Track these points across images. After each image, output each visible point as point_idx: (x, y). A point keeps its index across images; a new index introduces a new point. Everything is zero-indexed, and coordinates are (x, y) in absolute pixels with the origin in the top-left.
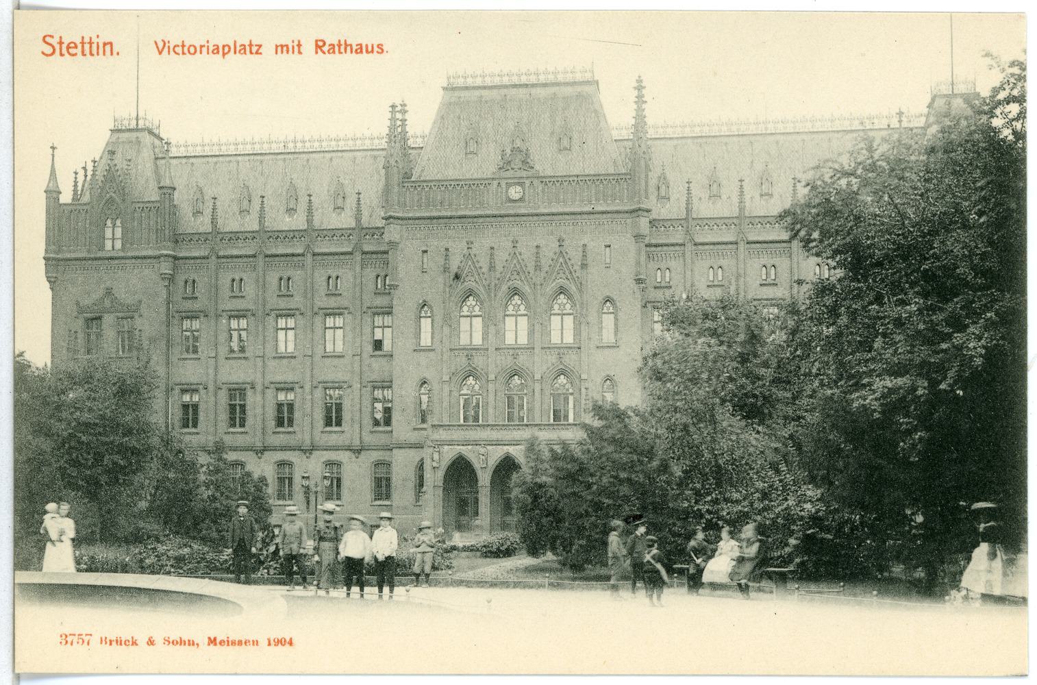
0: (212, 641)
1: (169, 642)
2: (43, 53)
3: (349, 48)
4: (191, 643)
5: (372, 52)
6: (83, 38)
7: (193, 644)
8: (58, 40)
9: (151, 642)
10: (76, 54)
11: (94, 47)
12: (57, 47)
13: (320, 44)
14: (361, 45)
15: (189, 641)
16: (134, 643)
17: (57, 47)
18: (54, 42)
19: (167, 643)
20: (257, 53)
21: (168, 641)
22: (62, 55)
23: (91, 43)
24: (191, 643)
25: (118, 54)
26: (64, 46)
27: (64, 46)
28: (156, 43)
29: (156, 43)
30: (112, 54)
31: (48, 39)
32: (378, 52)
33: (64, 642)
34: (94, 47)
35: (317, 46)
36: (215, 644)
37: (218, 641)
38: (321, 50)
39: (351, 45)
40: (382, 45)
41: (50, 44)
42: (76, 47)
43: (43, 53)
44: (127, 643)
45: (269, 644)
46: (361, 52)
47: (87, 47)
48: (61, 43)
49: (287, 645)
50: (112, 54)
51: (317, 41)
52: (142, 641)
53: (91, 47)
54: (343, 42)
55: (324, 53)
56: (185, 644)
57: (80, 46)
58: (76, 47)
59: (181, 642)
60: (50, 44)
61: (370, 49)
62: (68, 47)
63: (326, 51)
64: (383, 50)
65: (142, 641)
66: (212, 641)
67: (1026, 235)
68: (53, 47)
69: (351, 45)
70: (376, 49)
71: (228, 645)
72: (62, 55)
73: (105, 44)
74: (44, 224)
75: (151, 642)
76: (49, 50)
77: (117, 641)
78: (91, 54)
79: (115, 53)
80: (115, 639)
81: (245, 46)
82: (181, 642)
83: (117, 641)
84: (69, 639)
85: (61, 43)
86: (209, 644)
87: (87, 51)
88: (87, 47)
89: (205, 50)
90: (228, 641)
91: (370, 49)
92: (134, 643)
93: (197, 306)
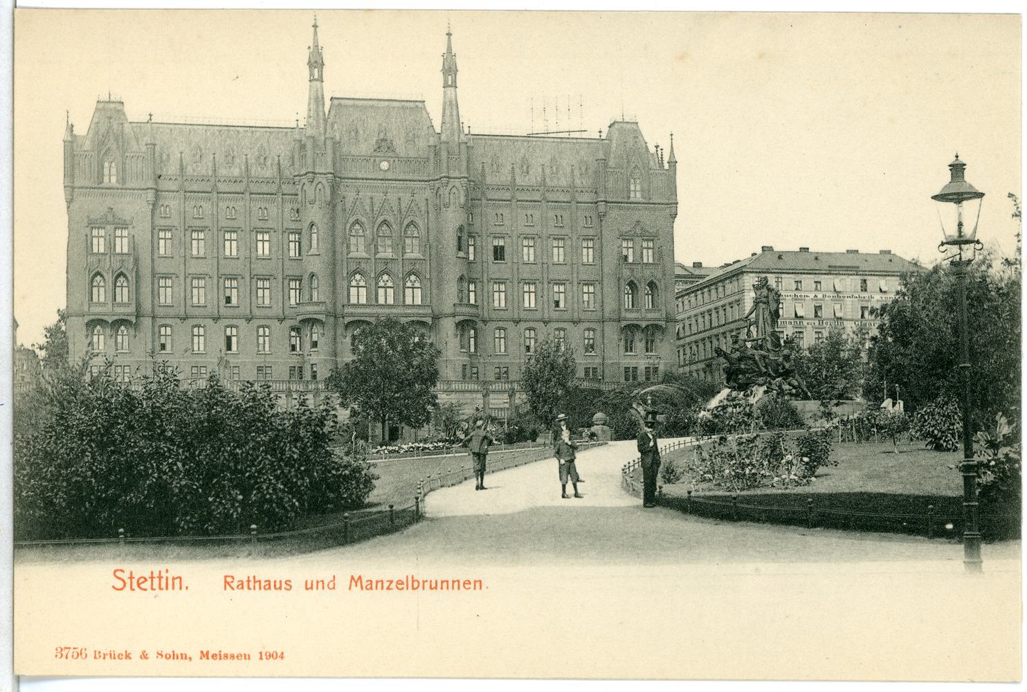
0: (204, 655)
1: (162, 656)
2: (113, 587)
4: (184, 657)
5: (280, 588)
6: (152, 573)
7: (186, 658)
8: (129, 575)
9: (144, 656)
10: (403, 588)
11: (163, 581)
12: (128, 582)
13: (229, 579)
14: (269, 581)
15: (182, 655)
16: (128, 656)
17: (128, 582)
18: (125, 576)
19: (160, 657)
21: (247, 657)
23: (160, 578)
24: (184, 657)
25: (187, 588)
26: (135, 581)
27: (135, 581)
30: (181, 588)
31: (118, 574)
32: (286, 589)
33: (59, 655)
34: (163, 581)
35: (226, 582)
36: (208, 658)
37: (210, 656)
38: (230, 586)
39: (260, 581)
40: (290, 581)
41: (119, 578)
43: (113, 587)
44: (121, 657)
45: (261, 658)
46: (270, 588)
47: (156, 581)
48: (131, 578)
49: (279, 659)
50: (181, 588)
51: (226, 577)
52: (136, 655)
53: (160, 580)
54: (252, 579)
55: (233, 589)
56: (177, 658)
58: (470, 583)
59: (174, 656)
60: (119, 578)
61: (278, 586)
62: (464, 583)
63: (235, 587)
64: (291, 587)
65: (136, 655)
66: (204, 655)
68: (123, 581)
69: (260, 581)
70: (284, 585)
71: (220, 659)
72: (132, 589)
73: (442, 582)
75: (144, 656)
76: (119, 584)
77: (111, 655)
78: (249, 588)
79: (184, 586)
80: (108, 653)
81: (371, 581)
82: (174, 656)
83: (111, 655)
84: (64, 653)
85: (131, 578)
86: (201, 658)
87: (163, 585)
89: (427, 585)
90: (220, 655)
91: (278, 586)
92: (128, 656)
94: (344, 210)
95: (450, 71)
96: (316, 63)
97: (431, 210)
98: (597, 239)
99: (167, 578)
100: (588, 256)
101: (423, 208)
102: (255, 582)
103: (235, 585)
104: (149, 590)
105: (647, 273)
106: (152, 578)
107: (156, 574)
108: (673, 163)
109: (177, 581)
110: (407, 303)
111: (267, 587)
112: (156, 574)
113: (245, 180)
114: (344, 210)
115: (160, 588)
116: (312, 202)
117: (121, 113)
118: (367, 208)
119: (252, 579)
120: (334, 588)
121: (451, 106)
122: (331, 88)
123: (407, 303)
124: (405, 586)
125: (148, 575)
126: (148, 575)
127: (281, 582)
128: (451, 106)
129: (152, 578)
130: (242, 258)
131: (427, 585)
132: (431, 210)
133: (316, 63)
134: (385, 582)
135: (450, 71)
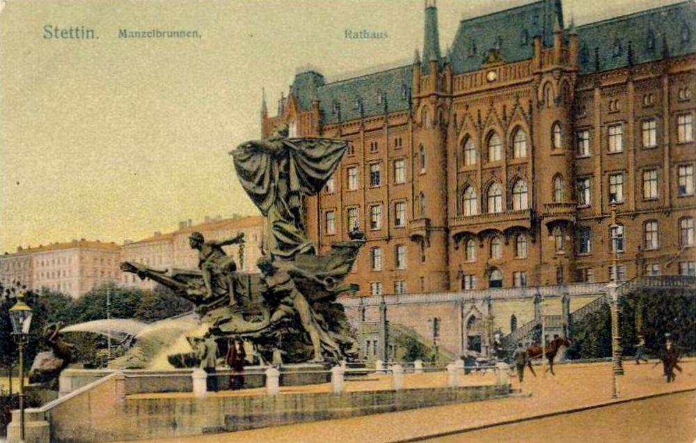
12: (54, 34)
17: (54, 34)
18: (52, 30)
26: (59, 33)
27: (59, 33)
48: (56, 30)
76: (48, 35)
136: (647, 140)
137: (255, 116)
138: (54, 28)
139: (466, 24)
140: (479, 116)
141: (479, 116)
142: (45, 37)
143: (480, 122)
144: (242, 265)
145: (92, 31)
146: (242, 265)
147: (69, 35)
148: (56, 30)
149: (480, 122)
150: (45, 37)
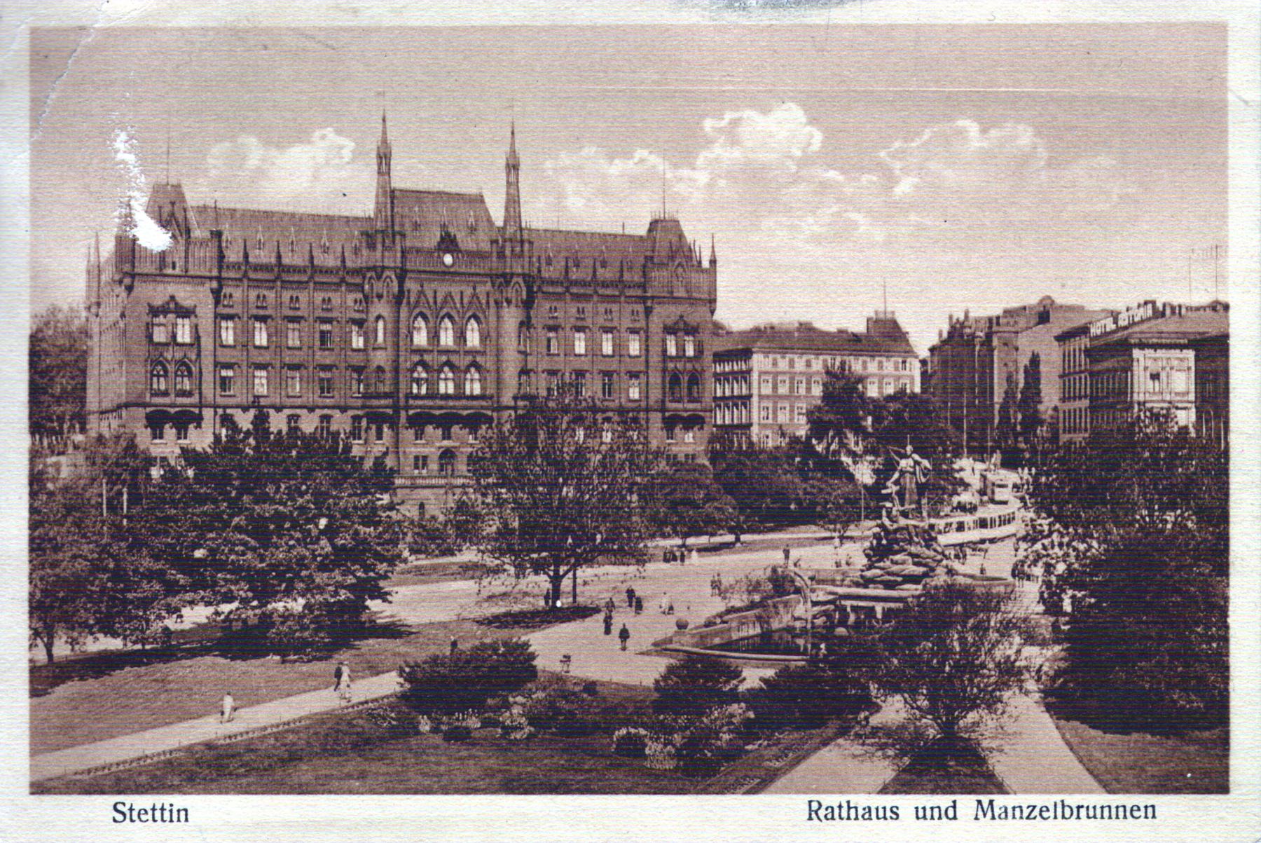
3: (853, 812)
12: (128, 813)
17: (128, 813)
18: (125, 810)
20: (1028, 818)
22: (132, 821)
23: (162, 809)
26: (135, 813)
27: (135, 813)
28: (187, 820)
29: (187, 820)
31: (120, 807)
42: (1139, 809)
47: (158, 814)
48: (131, 810)
57: (150, 813)
58: (1139, 809)
62: (1132, 810)
63: (822, 817)
64: (897, 815)
67: (221, 793)
70: (889, 814)
74: (576, 797)
76: (119, 817)
88: (158, 814)
93: (299, 313)
94: (409, 303)
95: (513, 167)
96: (384, 158)
97: (492, 304)
98: (644, 333)
99: (171, 811)
100: (634, 347)
101: (484, 302)
102: (849, 808)
103: (822, 813)
104: (1142, 819)
105: (689, 366)
106: (154, 809)
107: (158, 806)
108: (713, 262)
109: (183, 813)
110: (180, 340)
111: (867, 816)
112: (158, 806)
113: (309, 270)
114: (409, 303)
115: (841, 818)
116: (380, 297)
117: (181, 196)
118: (431, 300)
119: (845, 805)
120: (955, 818)
121: (513, 202)
122: (401, 179)
123: (180, 340)
124: (1051, 814)
125: (148, 808)
126: (148, 808)
127: (884, 808)
128: (513, 202)
129: (154, 809)
130: (273, 347)
131: (1083, 812)
132: (492, 304)
133: (384, 158)
134: (1024, 809)
135: (513, 167)
136: (96, 363)
137: (599, 674)
138: (128, 806)
139: (232, 416)
140: (435, 297)
141: (435, 297)
142: (115, 821)
143: (435, 303)
144: (594, 266)
145: (1153, 807)
146: (594, 266)
147: (149, 816)
148: (131, 810)
149: (435, 303)
150: (115, 821)
